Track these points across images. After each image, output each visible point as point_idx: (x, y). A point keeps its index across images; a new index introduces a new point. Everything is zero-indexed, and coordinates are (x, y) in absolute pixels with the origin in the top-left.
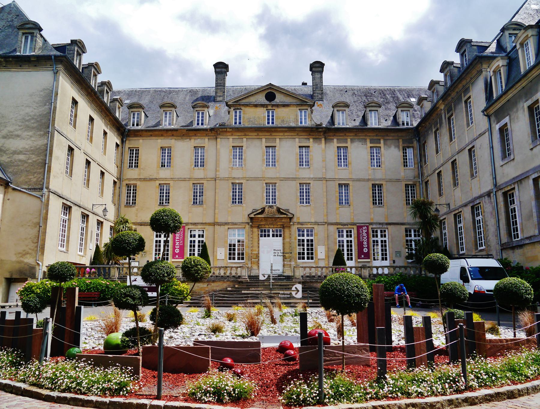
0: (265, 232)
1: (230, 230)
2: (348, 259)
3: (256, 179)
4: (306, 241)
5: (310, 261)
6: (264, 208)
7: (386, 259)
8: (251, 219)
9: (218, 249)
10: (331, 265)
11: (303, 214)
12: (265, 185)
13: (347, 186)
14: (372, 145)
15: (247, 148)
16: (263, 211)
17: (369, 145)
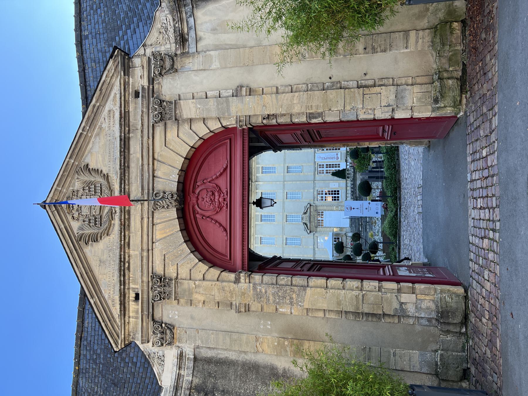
0: (319, 223)
1: (319, 247)
2: (339, 167)
3: (283, 229)
5: (340, 192)
8: (310, 232)
9: (421, 149)
16: (306, 224)
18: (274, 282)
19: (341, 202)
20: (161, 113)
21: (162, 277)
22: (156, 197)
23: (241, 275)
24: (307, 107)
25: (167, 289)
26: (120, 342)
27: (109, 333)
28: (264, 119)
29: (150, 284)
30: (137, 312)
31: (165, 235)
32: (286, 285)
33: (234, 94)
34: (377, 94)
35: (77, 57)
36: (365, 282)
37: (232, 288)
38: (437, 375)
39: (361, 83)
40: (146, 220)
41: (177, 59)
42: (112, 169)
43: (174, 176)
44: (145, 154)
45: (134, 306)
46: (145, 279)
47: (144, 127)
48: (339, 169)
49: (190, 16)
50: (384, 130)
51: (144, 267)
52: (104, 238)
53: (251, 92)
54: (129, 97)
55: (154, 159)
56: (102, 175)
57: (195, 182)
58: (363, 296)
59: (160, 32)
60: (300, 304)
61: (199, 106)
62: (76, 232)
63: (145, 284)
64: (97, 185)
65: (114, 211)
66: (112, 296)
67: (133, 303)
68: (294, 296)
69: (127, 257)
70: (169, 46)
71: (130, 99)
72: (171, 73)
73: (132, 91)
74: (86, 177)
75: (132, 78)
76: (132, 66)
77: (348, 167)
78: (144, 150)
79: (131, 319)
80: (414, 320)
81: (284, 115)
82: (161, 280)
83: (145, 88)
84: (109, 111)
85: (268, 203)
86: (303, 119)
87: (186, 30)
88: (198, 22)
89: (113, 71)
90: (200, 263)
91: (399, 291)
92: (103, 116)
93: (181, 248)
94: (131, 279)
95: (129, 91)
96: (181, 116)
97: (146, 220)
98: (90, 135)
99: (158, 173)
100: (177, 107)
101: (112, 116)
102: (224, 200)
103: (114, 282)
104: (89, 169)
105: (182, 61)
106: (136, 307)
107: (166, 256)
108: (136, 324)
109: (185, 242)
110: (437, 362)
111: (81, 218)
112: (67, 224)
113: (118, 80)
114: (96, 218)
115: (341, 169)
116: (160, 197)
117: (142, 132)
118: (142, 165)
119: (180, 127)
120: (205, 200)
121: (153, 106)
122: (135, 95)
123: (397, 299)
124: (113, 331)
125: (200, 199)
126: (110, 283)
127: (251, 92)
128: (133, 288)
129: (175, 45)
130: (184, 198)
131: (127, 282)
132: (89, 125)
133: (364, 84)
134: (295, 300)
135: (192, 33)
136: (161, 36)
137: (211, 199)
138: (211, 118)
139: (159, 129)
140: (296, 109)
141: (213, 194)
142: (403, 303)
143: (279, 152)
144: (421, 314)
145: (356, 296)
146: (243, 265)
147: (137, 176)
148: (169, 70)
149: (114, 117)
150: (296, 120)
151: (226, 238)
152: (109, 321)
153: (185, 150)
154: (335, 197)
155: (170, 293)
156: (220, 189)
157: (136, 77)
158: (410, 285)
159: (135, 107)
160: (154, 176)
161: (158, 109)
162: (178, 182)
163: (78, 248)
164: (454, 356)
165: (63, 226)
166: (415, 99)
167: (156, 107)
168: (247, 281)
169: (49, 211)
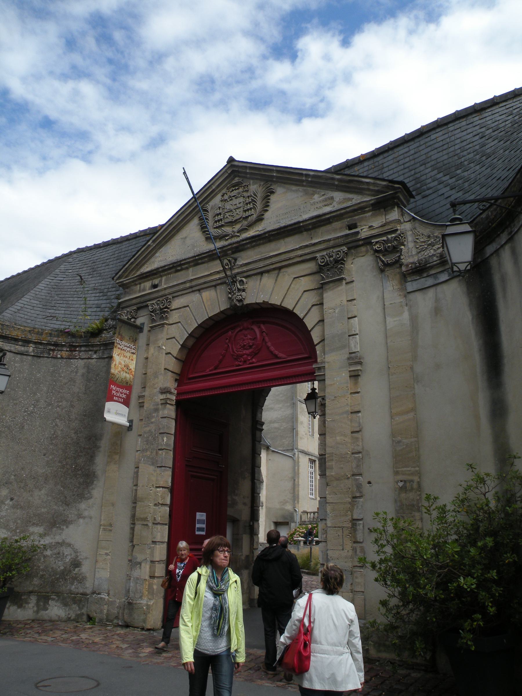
18: (161, 431)
27: (126, 268)
31: (205, 301)
34: (343, 545)
39: (360, 524)
42: (272, 221)
44: (283, 257)
45: (148, 285)
47: (312, 248)
53: (355, 376)
54: (349, 218)
55: (280, 268)
57: (264, 323)
58: (147, 525)
59: (429, 237)
61: (337, 311)
67: (150, 284)
68: (148, 453)
69: (185, 266)
70: (410, 255)
71: (346, 220)
74: (260, 196)
75: (371, 215)
78: (287, 254)
87: (433, 272)
88: (445, 287)
89: (376, 188)
90: (180, 347)
92: (327, 192)
98: (304, 184)
99: (265, 277)
101: (326, 203)
104: (269, 196)
106: (148, 288)
112: (217, 191)
118: (271, 257)
122: (352, 224)
127: (355, 376)
131: (166, 273)
135: (430, 282)
141: (251, 347)
142: (141, 565)
145: (147, 518)
148: (383, 261)
149: (325, 205)
153: (289, 304)
156: (256, 354)
161: (332, 259)
165: (214, 187)
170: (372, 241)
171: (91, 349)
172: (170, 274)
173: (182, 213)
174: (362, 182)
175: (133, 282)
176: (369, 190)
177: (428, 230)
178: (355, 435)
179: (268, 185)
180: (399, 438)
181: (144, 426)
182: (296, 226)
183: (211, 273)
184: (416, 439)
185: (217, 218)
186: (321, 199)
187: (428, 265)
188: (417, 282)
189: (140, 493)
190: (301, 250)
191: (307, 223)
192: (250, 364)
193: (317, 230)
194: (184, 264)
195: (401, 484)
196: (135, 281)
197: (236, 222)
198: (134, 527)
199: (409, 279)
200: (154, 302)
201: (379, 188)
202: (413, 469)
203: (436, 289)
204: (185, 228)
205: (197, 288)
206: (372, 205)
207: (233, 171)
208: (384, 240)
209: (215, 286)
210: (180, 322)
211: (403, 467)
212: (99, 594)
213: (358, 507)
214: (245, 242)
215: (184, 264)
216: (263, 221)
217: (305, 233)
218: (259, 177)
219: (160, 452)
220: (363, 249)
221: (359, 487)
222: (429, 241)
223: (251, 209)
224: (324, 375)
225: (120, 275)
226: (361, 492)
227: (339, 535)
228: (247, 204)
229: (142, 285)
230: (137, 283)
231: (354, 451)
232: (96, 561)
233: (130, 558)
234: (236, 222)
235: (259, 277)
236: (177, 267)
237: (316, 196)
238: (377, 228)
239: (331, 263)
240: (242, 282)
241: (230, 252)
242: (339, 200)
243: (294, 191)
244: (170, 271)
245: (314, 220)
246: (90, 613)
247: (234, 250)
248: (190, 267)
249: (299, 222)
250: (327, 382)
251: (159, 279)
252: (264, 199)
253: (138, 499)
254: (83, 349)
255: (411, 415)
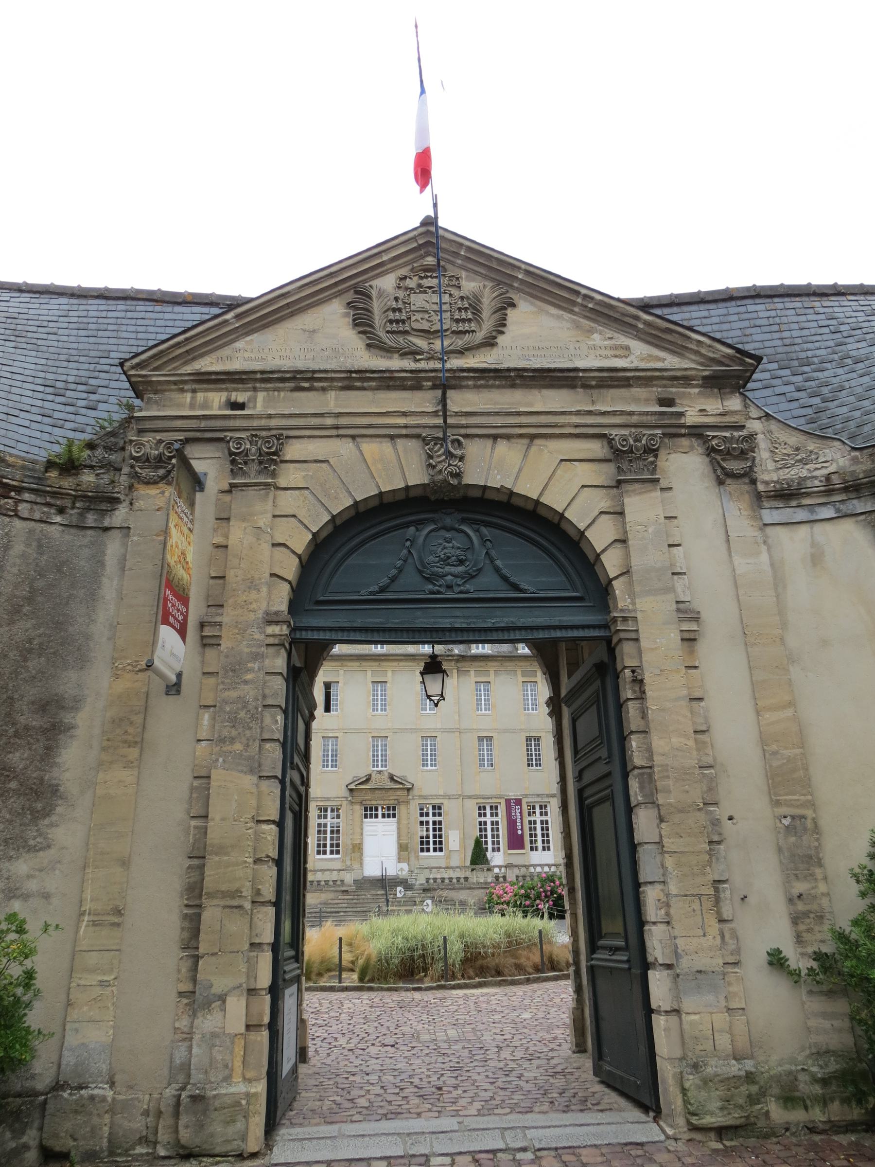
3: (358, 731)
4: (489, 824)
6: (370, 775)
7: (549, 849)
8: (351, 790)
10: (468, 864)
11: (428, 782)
12: (371, 739)
13: (491, 740)
14: (525, 679)
15: (344, 684)
16: (368, 780)
17: (521, 679)
18: (270, 702)
19: (418, 858)
20: (632, 452)
21: (279, 456)
22: (453, 442)
23: (285, 627)
24: (665, 767)
25: (255, 467)
26: (143, 372)
27: (162, 352)
28: (633, 672)
29: (264, 434)
30: (205, 406)
32: (262, 728)
33: (681, 606)
35: (728, 288)
36: (271, 911)
37: (254, 606)
38: (58, 1086)
39: (724, 889)
40: (401, 421)
41: (745, 484)
42: (509, 353)
43: (499, 477)
44: (543, 419)
45: (217, 400)
46: (273, 423)
48: (490, 849)
49: (838, 510)
50: (615, 950)
51: (302, 420)
52: (361, 338)
53: (690, 640)
55: (533, 437)
56: (494, 334)
57: (487, 524)
58: (240, 907)
59: (798, 449)
60: (221, 760)
62: (374, 283)
63: (263, 423)
64: (473, 325)
65: (418, 357)
66: (238, 355)
67: (224, 399)
68: (238, 747)
69: (371, 384)
71: (655, 389)
72: (715, 471)
73: (671, 393)
74: (487, 304)
75: (699, 393)
76: (725, 394)
77: (496, 870)
79: (189, 395)
80: (186, 1030)
81: (644, 714)
82: (274, 454)
83: (680, 419)
84: (627, 348)
85: (434, 688)
86: (637, 759)
88: (828, 526)
89: (711, 355)
90: (310, 537)
91: (252, 992)
92: (616, 335)
93: (343, 495)
94: (276, 393)
95: (672, 386)
96: (627, 491)
97: (401, 421)
99: (502, 446)
100: (646, 485)
101: (618, 353)
102: (449, 587)
103: (270, 358)
104: (505, 309)
105: (742, 494)
106: (216, 404)
107: (324, 465)
108: (180, 406)
109: (356, 503)
110: (87, 1087)
111: (401, 294)
112: (389, 266)
113: (694, 366)
114: (403, 322)
115: (489, 854)
116: (452, 450)
117: (590, 413)
118: (519, 414)
119: (604, 491)
120: (447, 545)
121: (644, 435)
122: (665, 399)
123: (234, 988)
124: (165, 359)
125: (448, 535)
126: (266, 351)
127: (690, 640)
128: (255, 398)
129: (775, 479)
130: (447, 502)
131: (269, 385)
132: (598, 308)
133: (722, 896)
134: (229, 748)
135: (801, 515)
136: (789, 451)
137: (449, 558)
138: (627, 556)
139: (596, 448)
140: (658, 743)
141: (461, 562)
142: (224, 1001)
143: (547, 710)
144: (199, 1046)
145: (239, 891)
146: (306, 629)
147: (495, 404)
148: (723, 468)
149: (616, 356)
150: (634, 744)
151: (363, 592)
152: (187, 351)
153: (555, 500)
154: (428, 843)
155: (244, 474)
156: (473, 577)
157: (702, 400)
158: (266, 1020)
159: (639, 399)
160: (495, 437)
161: (638, 444)
162: (485, 488)
163: (340, 288)
164: (101, 1129)
165: (385, 258)
166: (696, 1017)
167: (644, 442)
168: (271, 641)
169: (415, 233)
170: (708, 433)
171: (52, 501)
172: (278, 390)
173: (311, 282)
174: (689, 338)
175: (175, 383)
176: (697, 353)
177: (794, 439)
178: (700, 736)
179: (502, 291)
180: (774, 747)
181: (221, 687)
182: (571, 374)
183: (387, 412)
184: (801, 750)
185: (391, 316)
186: (606, 343)
187: (803, 490)
188: (780, 511)
189: (214, 835)
190: (578, 416)
191: (592, 374)
192: (461, 592)
193: (604, 391)
194: (320, 380)
195: (786, 822)
196: (185, 382)
197: (439, 333)
198: (199, 915)
199: (766, 504)
200: (243, 435)
201: (715, 356)
202: (802, 797)
203: (812, 528)
204: (309, 311)
205: (352, 431)
206: (704, 378)
207: (428, 243)
208: (725, 437)
209: (392, 437)
210: (307, 488)
211: (787, 795)
212: (80, 1087)
213: (717, 859)
214: (465, 374)
215: (320, 380)
216: (495, 349)
217: (580, 390)
218: (484, 272)
219: (268, 746)
220: (685, 442)
221: (716, 823)
222: (797, 455)
223: (470, 320)
224: (637, 631)
225: (144, 361)
226: (720, 834)
227: (694, 910)
228: (460, 309)
229: (200, 396)
230: (186, 387)
231: (701, 764)
232: (69, 1004)
233: (186, 987)
234: (439, 333)
235: (489, 442)
236: (301, 380)
237: (596, 338)
238: (712, 415)
239: (638, 450)
240: (456, 444)
241: (430, 384)
242: (639, 354)
243: (552, 315)
244: (281, 385)
245: (605, 374)
246: (48, 1143)
247: (438, 383)
248: (332, 388)
249: (576, 370)
250: (644, 643)
251: (249, 394)
252: (495, 312)
253: (209, 848)
254: (27, 496)
255: (789, 713)
